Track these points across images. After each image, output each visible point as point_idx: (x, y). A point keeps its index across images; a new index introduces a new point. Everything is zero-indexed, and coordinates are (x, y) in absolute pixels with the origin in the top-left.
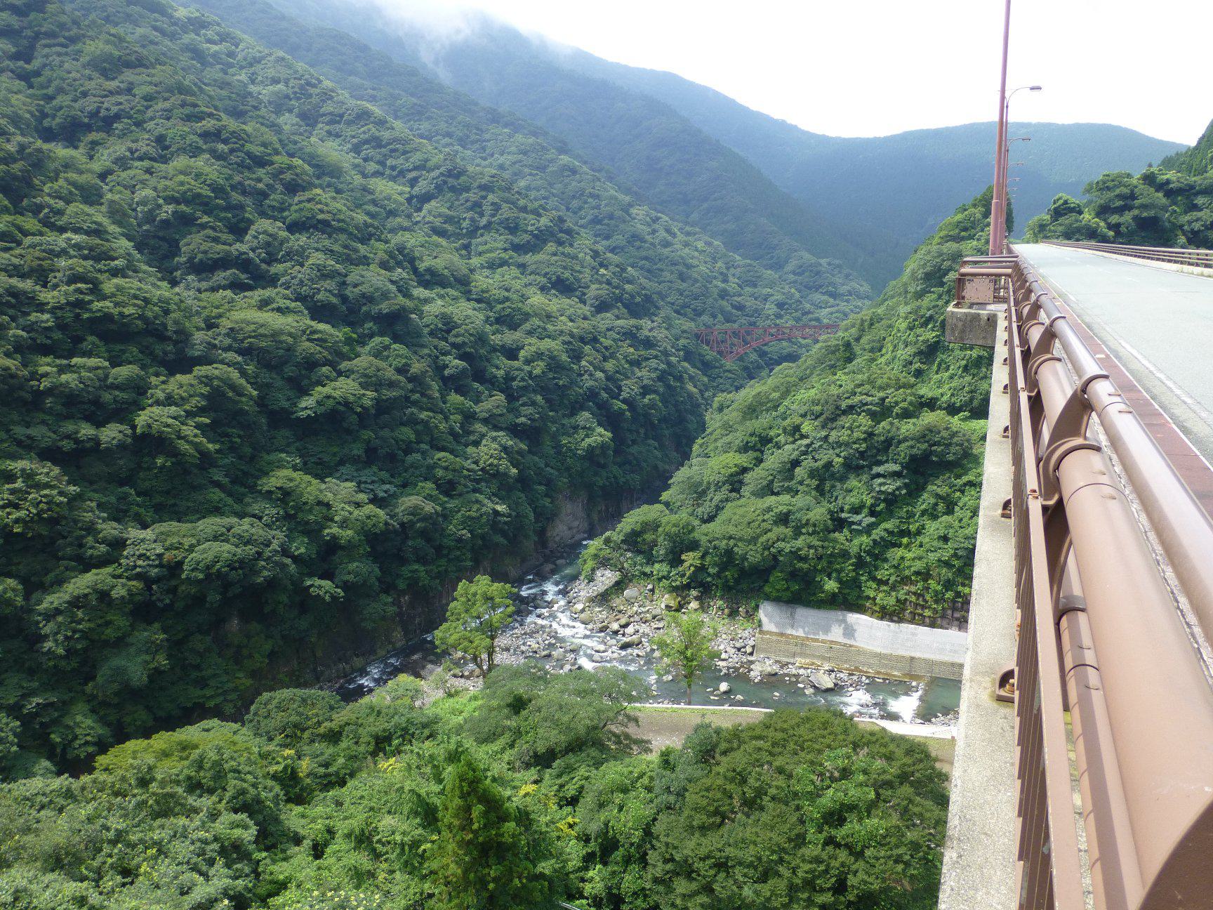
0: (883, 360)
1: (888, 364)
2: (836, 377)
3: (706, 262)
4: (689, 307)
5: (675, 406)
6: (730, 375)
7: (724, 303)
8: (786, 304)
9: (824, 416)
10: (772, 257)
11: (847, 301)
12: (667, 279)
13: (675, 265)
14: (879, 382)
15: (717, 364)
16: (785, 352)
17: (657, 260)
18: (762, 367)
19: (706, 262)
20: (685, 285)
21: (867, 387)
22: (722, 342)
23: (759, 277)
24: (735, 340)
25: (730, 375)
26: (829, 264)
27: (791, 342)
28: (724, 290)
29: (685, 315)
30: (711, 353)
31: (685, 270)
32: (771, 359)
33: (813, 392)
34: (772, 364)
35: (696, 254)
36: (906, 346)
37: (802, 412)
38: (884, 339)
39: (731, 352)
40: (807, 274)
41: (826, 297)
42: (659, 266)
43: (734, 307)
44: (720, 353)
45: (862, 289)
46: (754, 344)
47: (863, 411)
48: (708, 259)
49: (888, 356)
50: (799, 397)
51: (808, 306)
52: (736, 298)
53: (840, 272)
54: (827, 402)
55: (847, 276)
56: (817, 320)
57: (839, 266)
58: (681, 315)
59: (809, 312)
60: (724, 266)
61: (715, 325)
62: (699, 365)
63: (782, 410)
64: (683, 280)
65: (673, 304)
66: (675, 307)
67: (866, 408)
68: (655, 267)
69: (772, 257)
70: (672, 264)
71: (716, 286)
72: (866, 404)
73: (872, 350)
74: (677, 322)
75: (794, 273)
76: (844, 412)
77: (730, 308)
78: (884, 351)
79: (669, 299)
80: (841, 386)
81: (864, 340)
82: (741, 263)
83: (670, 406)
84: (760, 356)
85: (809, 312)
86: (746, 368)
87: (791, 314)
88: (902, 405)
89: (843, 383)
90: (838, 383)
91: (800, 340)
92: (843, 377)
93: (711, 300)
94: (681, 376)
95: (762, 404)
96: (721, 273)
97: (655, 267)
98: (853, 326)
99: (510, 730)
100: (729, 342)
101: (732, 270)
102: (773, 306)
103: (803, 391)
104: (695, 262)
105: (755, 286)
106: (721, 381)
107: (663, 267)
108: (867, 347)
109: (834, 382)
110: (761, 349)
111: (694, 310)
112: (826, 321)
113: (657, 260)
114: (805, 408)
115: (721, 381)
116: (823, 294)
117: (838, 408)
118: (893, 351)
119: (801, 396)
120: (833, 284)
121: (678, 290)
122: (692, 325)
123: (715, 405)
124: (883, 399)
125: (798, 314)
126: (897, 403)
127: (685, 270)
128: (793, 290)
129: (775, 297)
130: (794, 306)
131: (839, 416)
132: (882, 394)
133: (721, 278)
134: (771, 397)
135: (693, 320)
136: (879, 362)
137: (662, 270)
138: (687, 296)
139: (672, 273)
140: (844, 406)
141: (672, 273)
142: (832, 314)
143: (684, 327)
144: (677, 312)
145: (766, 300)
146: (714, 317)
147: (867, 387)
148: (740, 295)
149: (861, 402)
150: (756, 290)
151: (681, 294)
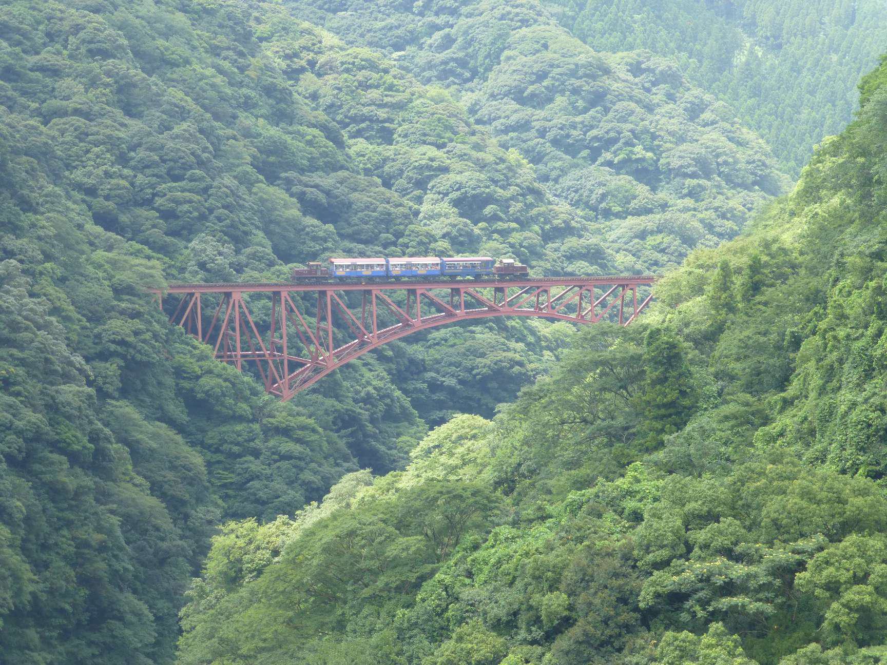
0: (786, 421)
1: (807, 435)
2: (622, 483)
3: (215, 51)
4: (147, 203)
5: (75, 561)
6: (288, 446)
7: (276, 193)
8: (489, 199)
9: (575, 632)
10: (448, 42)
11: (693, 194)
12: (71, 105)
13: (105, 54)
14: (772, 507)
15: (243, 408)
16: (484, 364)
17: (39, 37)
18: (406, 416)
19: (215, 51)
20: (135, 125)
21: (728, 524)
22: (263, 328)
23: (400, 106)
24: (307, 323)
25: (288, 446)
26: (636, 69)
27: (503, 329)
28: (277, 149)
29: (133, 232)
30: (219, 365)
31: (136, 73)
32: (434, 386)
33: (542, 533)
34: (441, 405)
35: (181, 19)
36: (868, 375)
37: (498, 611)
38: (796, 342)
39: (293, 366)
40: (560, 101)
41: (624, 181)
42: (47, 56)
43: (309, 206)
44: (255, 367)
45: (742, 155)
46: (373, 338)
47: (714, 616)
48: (222, 40)
49: (808, 407)
50: (490, 554)
51: (563, 208)
52: (316, 178)
53: (671, 97)
54: (586, 580)
55: (694, 111)
56: (595, 255)
57: (671, 78)
58: (120, 230)
59: (567, 230)
60: (280, 64)
61: (239, 269)
62: (176, 410)
63: (432, 603)
64: (130, 110)
65: (91, 191)
66: (99, 203)
67: (725, 602)
68: (32, 60)
69: (448, 42)
70: (92, 53)
71: (247, 134)
72: (729, 588)
73: (756, 384)
74: (100, 255)
75: (519, 96)
76: (648, 617)
77: (294, 212)
78: (792, 390)
79: (77, 175)
80: (637, 517)
81: (727, 343)
82: (339, 57)
83: (58, 563)
84: (399, 378)
85: (567, 230)
86: (345, 421)
87: (504, 233)
88: (851, 595)
89: (647, 508)
90: (630, 504)
91: (535, 323)
92: (648, 485)
93: (228, 180)
94: (100, 454)
95: (358, 577)
96: (269, 91)
97: (32, 60)
98: (698, 290)
99: (537, 621)
100: (286, 329)
101: (308, 81)
102: (445, 207)
103: (505, 531)
104: (175, 48)
105: (387, 136)
106: (255, 466)
107: (61, 61)
108: (736, 367)
109: (613, 503)
110: (399, 353)
111: (168, 215)
112: (622, 260)
113: (39, 37)
114: (510, 597)
115: (255, 466)
116: (618, 168)
117: (625, 599)
118: (822, 391)
119: (500, 551)
120: (651, 138)
121: (111, 143)
122: (156, 266)
123: (214, 565)
124: (786, 572)
125: (532, 235)
126: (834, 588)
127: (136, 73)
128: (513, 155)
129: (453, 177)
130: (516, 207)
131: (628, 628)
132: (781, 554)
133: (265, 105)
134: (392, 551)
135: (163, 249)
136: (774, 428)
137: (55, 72)
138: (144, 166)
139: (93, 83)
140: (645, 598)
141: (93, 83)
142: (642, 235)
143: (124, 277)
144: (106, 220)
145: (421, 184)
146: (238, 239)
147: (728, 524)
148: (334, 167)
149: (706, 580)
150: (388, 151)
151: (123, 160)
